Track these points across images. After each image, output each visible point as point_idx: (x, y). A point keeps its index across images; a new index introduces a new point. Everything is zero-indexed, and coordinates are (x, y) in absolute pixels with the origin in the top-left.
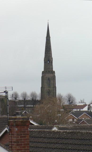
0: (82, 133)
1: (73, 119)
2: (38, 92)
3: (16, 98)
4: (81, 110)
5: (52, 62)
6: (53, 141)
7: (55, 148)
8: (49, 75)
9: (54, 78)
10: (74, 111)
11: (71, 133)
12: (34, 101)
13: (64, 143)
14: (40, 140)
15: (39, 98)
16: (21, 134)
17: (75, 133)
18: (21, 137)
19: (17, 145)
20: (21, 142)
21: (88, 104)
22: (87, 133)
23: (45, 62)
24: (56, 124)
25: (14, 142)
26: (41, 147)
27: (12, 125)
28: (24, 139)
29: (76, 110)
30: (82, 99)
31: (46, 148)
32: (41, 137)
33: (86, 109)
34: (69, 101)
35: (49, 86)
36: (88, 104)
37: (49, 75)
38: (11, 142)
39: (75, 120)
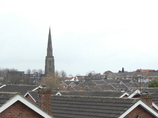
0: (81, 97)
1: (66, 87)
2: (43, 69)
3: (29, 73)
4: (70, 80)
5: (52, 51)
6: (64, 102)
7: (65, 107)
8: (51, 59)
9: (53, 61)
10: (66, 81)
11: (74, 97)
12: (42, 75)
13: (71, 103)
14: (55, 101)
15: (43, 73)
16: (47, 99)
17: (77, 97)
18: (46, 100)
19: (44, 105)
20: (46, 103)
21: (74, 76)
22: (85, 97)
23: (48, 51)
24: (58, 90)
25: (42, 103)
26: (56, 106)
27: (41, 93)
28: (48, 102)
29: (67, 80)
30: (71, 74)
31: (59, 106)
32: (56, 100)
33: (73, 80)
34: (63, 75)
35: (50, 65)
36: (74, 76)
37: (51, 59)
38: (40, 103)
39: (67, 87)
